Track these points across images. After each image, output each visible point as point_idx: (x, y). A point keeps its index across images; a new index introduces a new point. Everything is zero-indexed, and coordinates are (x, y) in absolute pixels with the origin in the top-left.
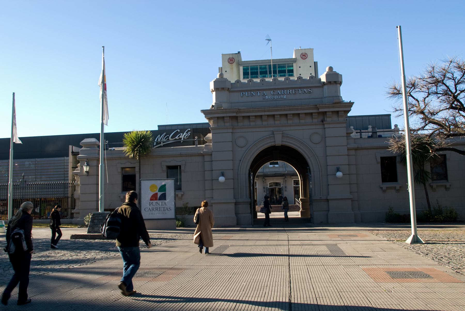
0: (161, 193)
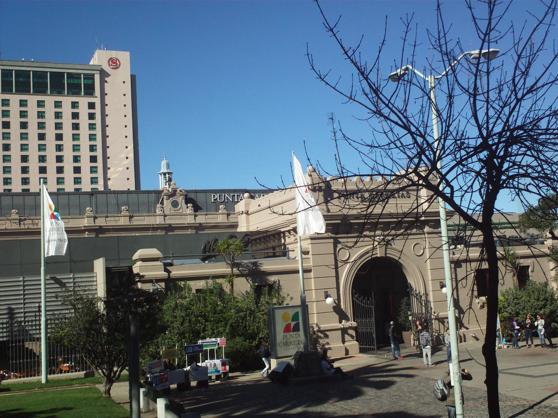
0: (295, 323)
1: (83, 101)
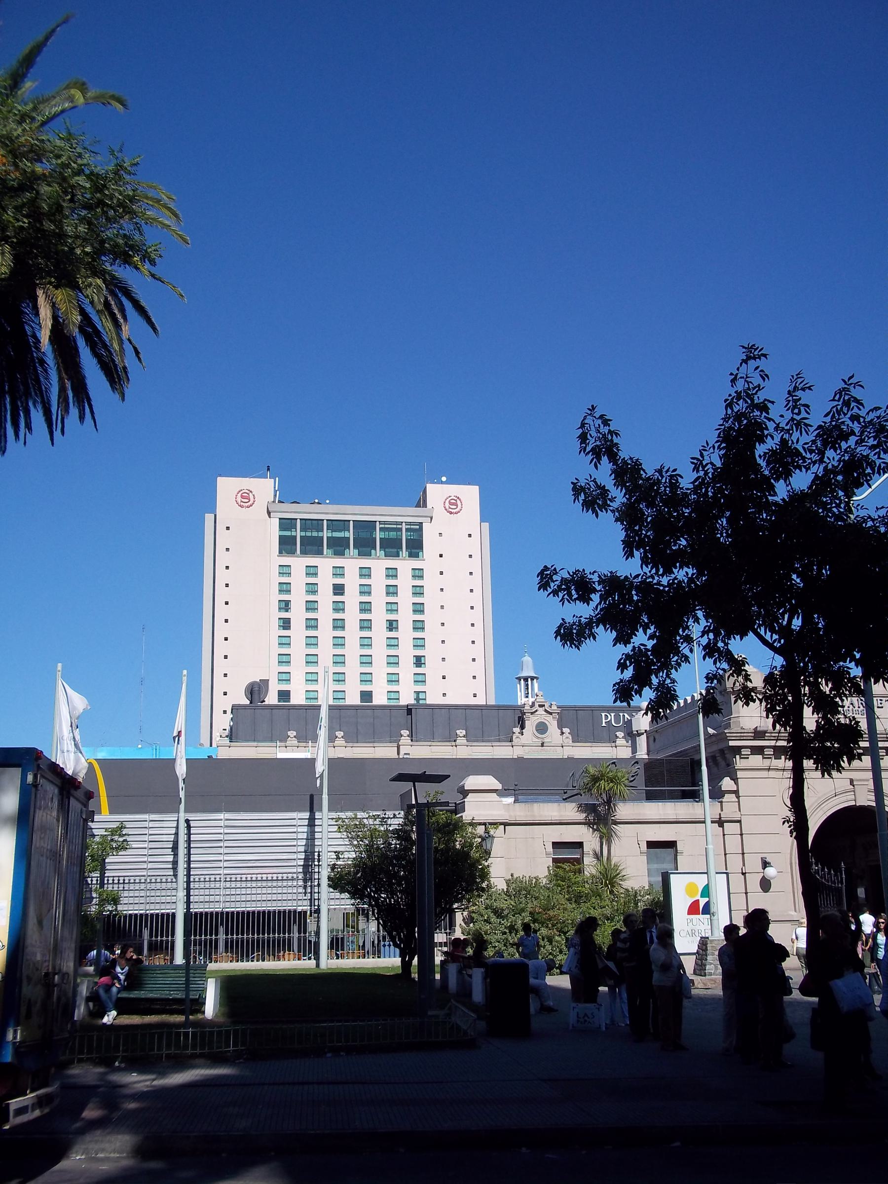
1: (404, 565)
